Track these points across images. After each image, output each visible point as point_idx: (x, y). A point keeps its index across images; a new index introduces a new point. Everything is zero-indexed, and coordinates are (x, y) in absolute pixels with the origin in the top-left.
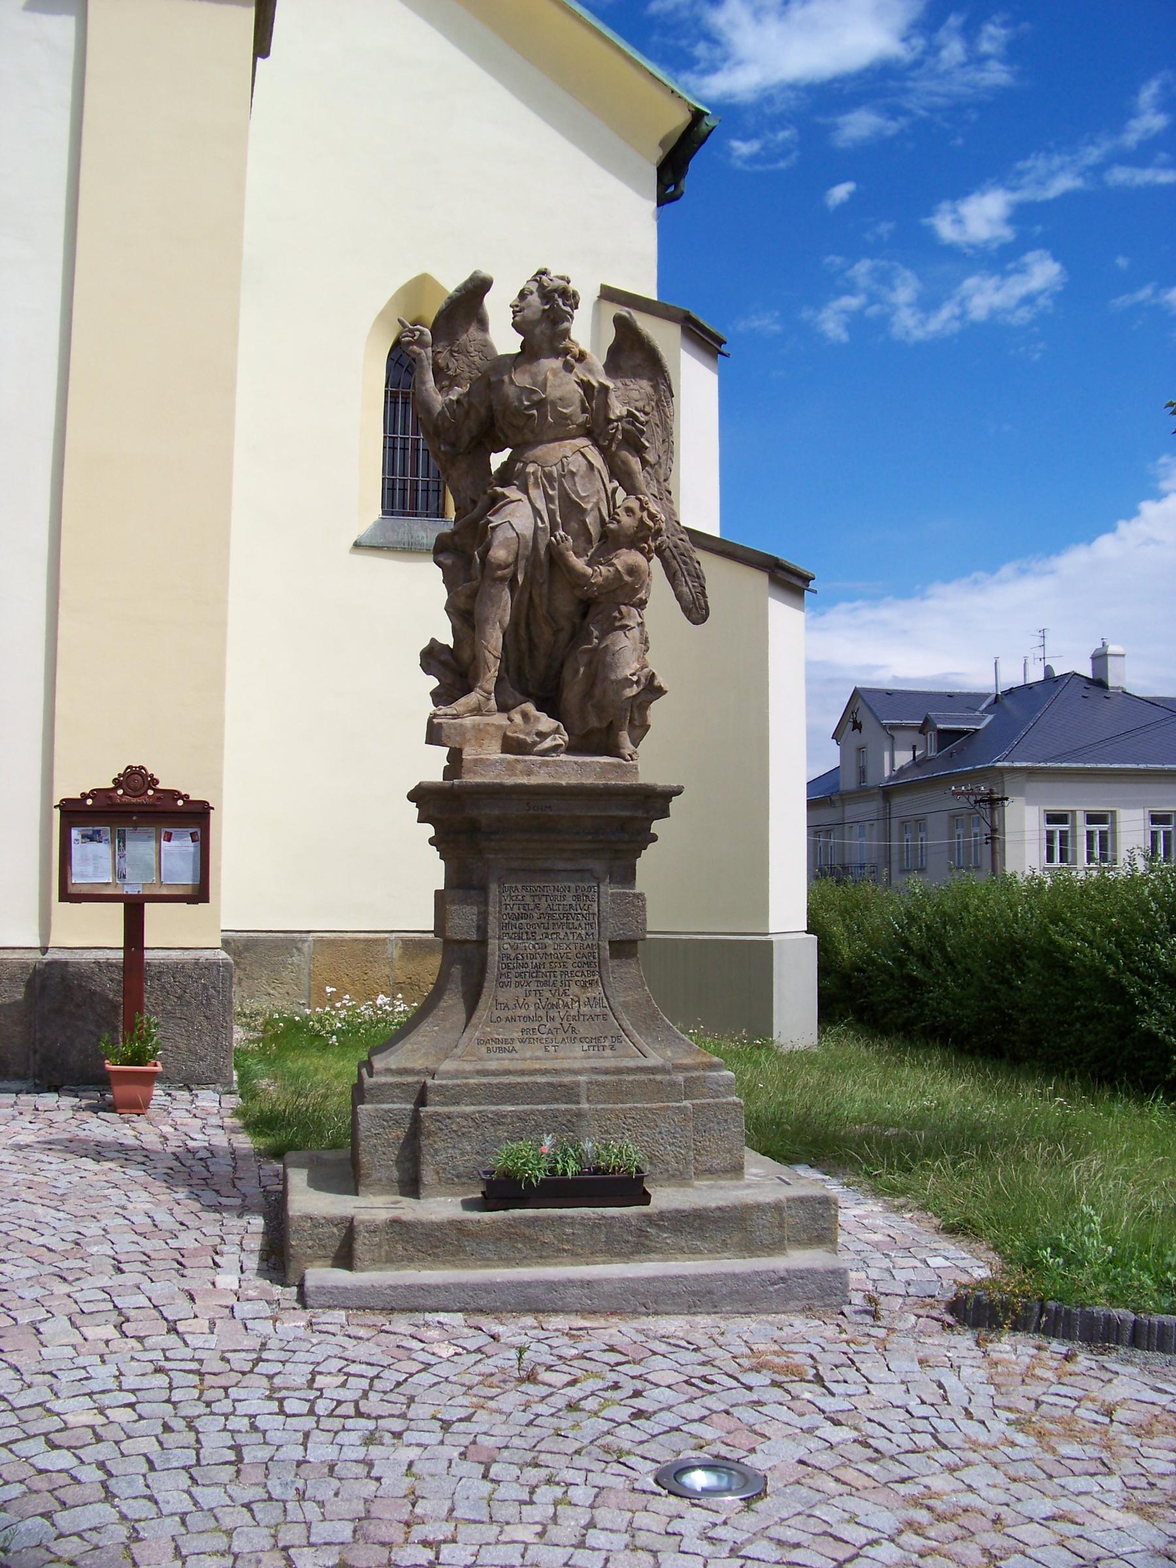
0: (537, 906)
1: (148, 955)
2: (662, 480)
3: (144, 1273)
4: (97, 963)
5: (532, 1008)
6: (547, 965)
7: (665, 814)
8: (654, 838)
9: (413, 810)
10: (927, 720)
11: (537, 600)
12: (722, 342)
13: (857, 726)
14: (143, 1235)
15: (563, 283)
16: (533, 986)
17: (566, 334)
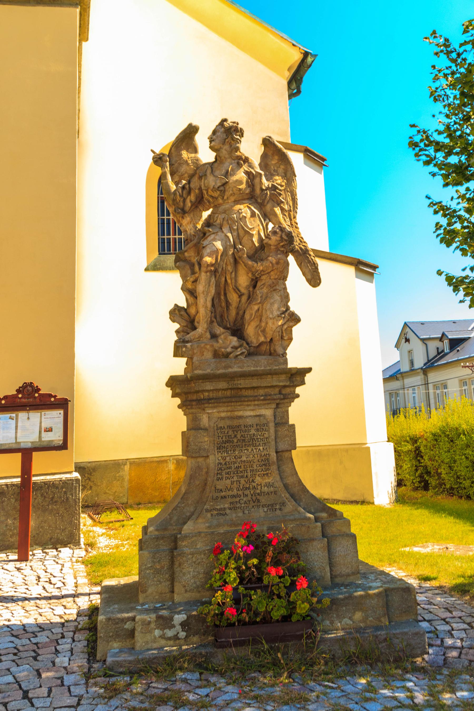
0: (235, 436)
1: (34, 479)
2: (292, 218)
3: (13, 661)
4: (7, 485)
5: (235, 490)
6: (242, 467)
7: (303, 383)
8: (298, 396)
9: (169, 391)
10: (443, 334)
11: (229, 281)
12: (324, 160)
13: (407, 340)
14: (16, 636)
15: (235, 125)
16: (235, 479)
17: (237, 149)
